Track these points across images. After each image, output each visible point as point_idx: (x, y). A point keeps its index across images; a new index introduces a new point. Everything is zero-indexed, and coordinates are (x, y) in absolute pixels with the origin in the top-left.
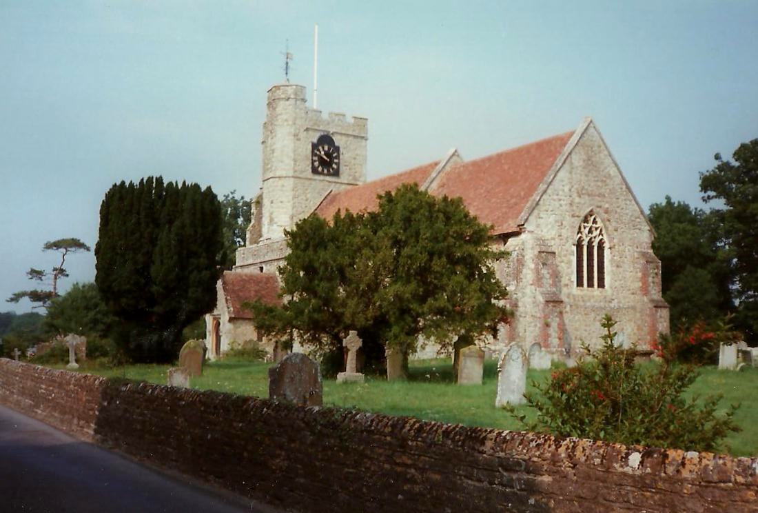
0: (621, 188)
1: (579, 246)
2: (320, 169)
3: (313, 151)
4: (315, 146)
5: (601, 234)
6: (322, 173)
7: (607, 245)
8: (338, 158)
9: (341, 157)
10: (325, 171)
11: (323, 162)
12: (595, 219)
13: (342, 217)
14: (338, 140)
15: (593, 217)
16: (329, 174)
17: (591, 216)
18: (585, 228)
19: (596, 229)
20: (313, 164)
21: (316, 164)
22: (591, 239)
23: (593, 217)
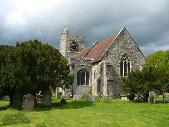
0: (135, 47)
1: (121, 64)
2: (72, 50)
3: (77, 49)
4: (71, 44)
5: (129, 60)
6: (73, 51)
7: (131, 64)
8: (77, 47)
9: (78, 46)
10: (74, 50)
11: (73, 48)
12: (127, 56)
13: (68, 75)
14: (77, 43)
15: (126, 56)
16: (75, 51)
17: (125, 55)
18: (123, 59)
19: (127, 59)
20: (70, 48)
21: (72, 48)
22: (125, 62)
23: (126, 56)
